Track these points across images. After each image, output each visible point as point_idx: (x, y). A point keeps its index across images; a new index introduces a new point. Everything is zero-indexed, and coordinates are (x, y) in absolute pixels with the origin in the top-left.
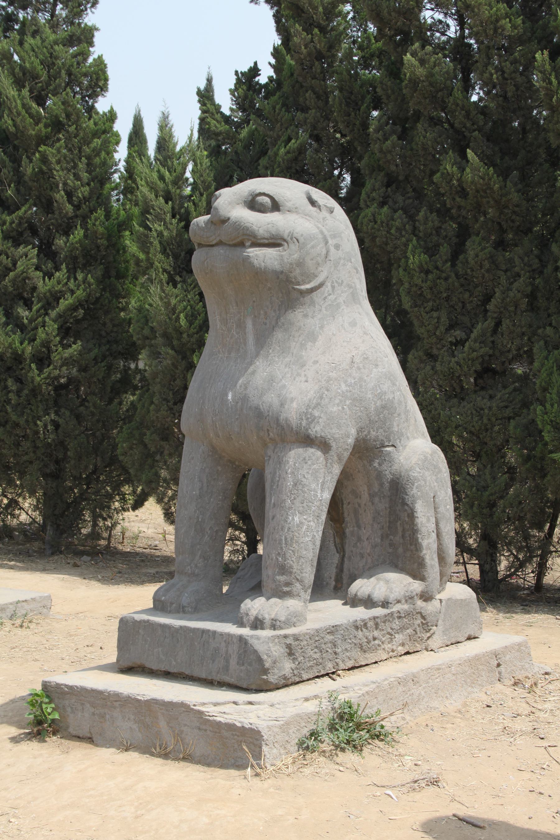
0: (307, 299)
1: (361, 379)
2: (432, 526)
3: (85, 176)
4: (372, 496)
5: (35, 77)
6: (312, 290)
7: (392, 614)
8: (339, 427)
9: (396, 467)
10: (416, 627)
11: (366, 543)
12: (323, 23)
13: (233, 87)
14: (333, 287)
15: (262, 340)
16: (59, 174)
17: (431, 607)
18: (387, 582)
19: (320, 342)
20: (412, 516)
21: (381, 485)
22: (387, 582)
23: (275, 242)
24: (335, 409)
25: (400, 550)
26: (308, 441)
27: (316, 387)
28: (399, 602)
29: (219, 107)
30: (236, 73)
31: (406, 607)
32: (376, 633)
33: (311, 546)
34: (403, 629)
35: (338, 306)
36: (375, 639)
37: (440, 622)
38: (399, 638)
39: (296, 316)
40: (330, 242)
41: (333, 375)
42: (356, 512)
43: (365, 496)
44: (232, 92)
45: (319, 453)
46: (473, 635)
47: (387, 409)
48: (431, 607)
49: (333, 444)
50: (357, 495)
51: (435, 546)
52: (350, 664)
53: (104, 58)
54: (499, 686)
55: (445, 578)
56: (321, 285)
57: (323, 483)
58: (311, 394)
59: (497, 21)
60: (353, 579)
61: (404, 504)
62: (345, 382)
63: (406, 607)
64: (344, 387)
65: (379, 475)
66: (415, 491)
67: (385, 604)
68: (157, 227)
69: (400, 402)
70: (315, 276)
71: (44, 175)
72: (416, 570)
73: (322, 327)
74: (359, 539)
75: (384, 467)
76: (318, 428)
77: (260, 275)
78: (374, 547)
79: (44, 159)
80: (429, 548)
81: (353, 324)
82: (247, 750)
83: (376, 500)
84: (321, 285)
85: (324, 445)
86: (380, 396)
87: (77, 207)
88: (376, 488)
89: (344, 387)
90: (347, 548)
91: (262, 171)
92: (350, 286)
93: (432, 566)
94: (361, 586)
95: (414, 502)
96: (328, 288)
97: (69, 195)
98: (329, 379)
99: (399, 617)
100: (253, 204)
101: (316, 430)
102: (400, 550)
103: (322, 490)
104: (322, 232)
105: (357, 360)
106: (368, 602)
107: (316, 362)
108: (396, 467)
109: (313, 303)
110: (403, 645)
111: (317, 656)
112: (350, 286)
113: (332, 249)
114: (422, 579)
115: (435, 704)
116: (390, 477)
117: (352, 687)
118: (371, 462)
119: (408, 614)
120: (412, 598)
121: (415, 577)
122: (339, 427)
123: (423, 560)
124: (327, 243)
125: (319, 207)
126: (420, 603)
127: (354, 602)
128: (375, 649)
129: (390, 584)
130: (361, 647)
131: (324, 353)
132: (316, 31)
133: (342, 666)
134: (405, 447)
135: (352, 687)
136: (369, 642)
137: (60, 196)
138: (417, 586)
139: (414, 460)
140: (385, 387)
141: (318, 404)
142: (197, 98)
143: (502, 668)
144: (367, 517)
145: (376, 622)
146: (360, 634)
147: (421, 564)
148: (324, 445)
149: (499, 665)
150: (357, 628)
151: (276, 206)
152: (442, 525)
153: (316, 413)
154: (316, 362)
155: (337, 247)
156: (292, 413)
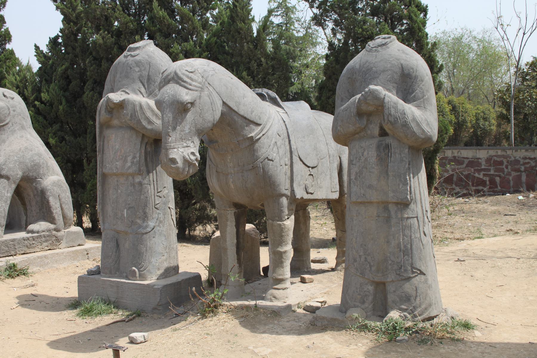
0: (2, 128)
1: (23, 155)
2: (58, 205)
4: (34, 195)
6: (3, 126)
7: (41, 236)
8: (13, 171)
9: (42, 186)
10: (53, 241)
11: (34, 212)
12: (75, 21)
13: (48, 44)
14: (13, 125)
17: (59, 234)
18: (40, 225)
19: (7, 143)
20: (48, 202)
21: (37, 192)
22: (40, 225)
24: (12, 165)
25: (46, 214)
27: (4, 158)
28: (44, 231)
29: (42, 51)
30: (50, 38)
31: (47, 233)
32: (34, 242)
33: (3, 212)
34: (46, 241)
35: (15, 131)
36: (33, 244)
37: (64, 239)
38: (45, 244)
40: (11, 109)
41: (12, 154)
42: (30, 201)
43: (32, 195)
44: (47, 46)
45: (6, 181)
46: (81, 244)
47: (36, 166)
48: (59, 234)
49: (11, 178)
50: (29, 195)
51: (60, 213)
52: (23, 252)
53: (10, 30)
54: (87, 261)
55: (66, 224)
56: (7, 124)
57: (7, 191)
58: (2, 161)
59: (127, 24)
60: (30, 224)
61: (45, 198)
62: (17, 156)
63: (47, 233)
64: (16, 158)
65: (36, 188)
66: (49, 193)
67: (38, 232)
69: (43, 163)
70: (5, 121)
72: (52, 220)
73: (8, 138)
74: (32, 211)
75: (38, 185)
76: (4, 172)
78: (37, 213)
80: (56, 213)
81: (22, 137)
82: (253, 303)
83: (36, 197)
84: (7, 124)
85: (7, 178)
86: (33, 161)
88: (36, 193)
89: (16, 158)
90: (28, 214)
91: (172, 57)
92: (20, 124)
93: (59, 220)
94: (31, 227)
95: (48, 197)
96: (10, 124)
98: (10, 156)
99: (44, 237)
102: (46, 214)
103: (7, 193)
104: (7, 106)
105: (22, 149)
106: (32, 232)
107: (5, 150)
108: (42, 186)
109: (4, 130)
110: (47, 246)
111: (7, 249)
112: (20, 124)
113: (12, 112)
114: (55, 224)
115: (55, 265)
116: (40, 189)
117: (18, 260)
118: (32, 184)
119: (48, 236)
120: (50, 230)
121: (52, 223)
122: (13, 171)
123: (54, 217)
124: (9, 109)
125: (7, 97)
126: (54, 232)
127: (28, 232)
128: (34, 247)
129: (41, 226)
130: (27, 247)
131: (8, 147)
132: (72, 24)
133: (19, 253)
134: (46, 179)
135: (18, 260)
136: (30, 245)
138: (52, 226)
139: (49, 183)
140: (35, 158)
141: (4, 164)
142: (34, 47)
143: (89, 255)
144: (34, 203)
145: (37, 237)
146: (26, 242)
147: (54, 219)
149: (87, 254)
150: (24, 240)
152: (63, 206)
153: (4, 167)
154: (5, 150)
155: (14, 111)
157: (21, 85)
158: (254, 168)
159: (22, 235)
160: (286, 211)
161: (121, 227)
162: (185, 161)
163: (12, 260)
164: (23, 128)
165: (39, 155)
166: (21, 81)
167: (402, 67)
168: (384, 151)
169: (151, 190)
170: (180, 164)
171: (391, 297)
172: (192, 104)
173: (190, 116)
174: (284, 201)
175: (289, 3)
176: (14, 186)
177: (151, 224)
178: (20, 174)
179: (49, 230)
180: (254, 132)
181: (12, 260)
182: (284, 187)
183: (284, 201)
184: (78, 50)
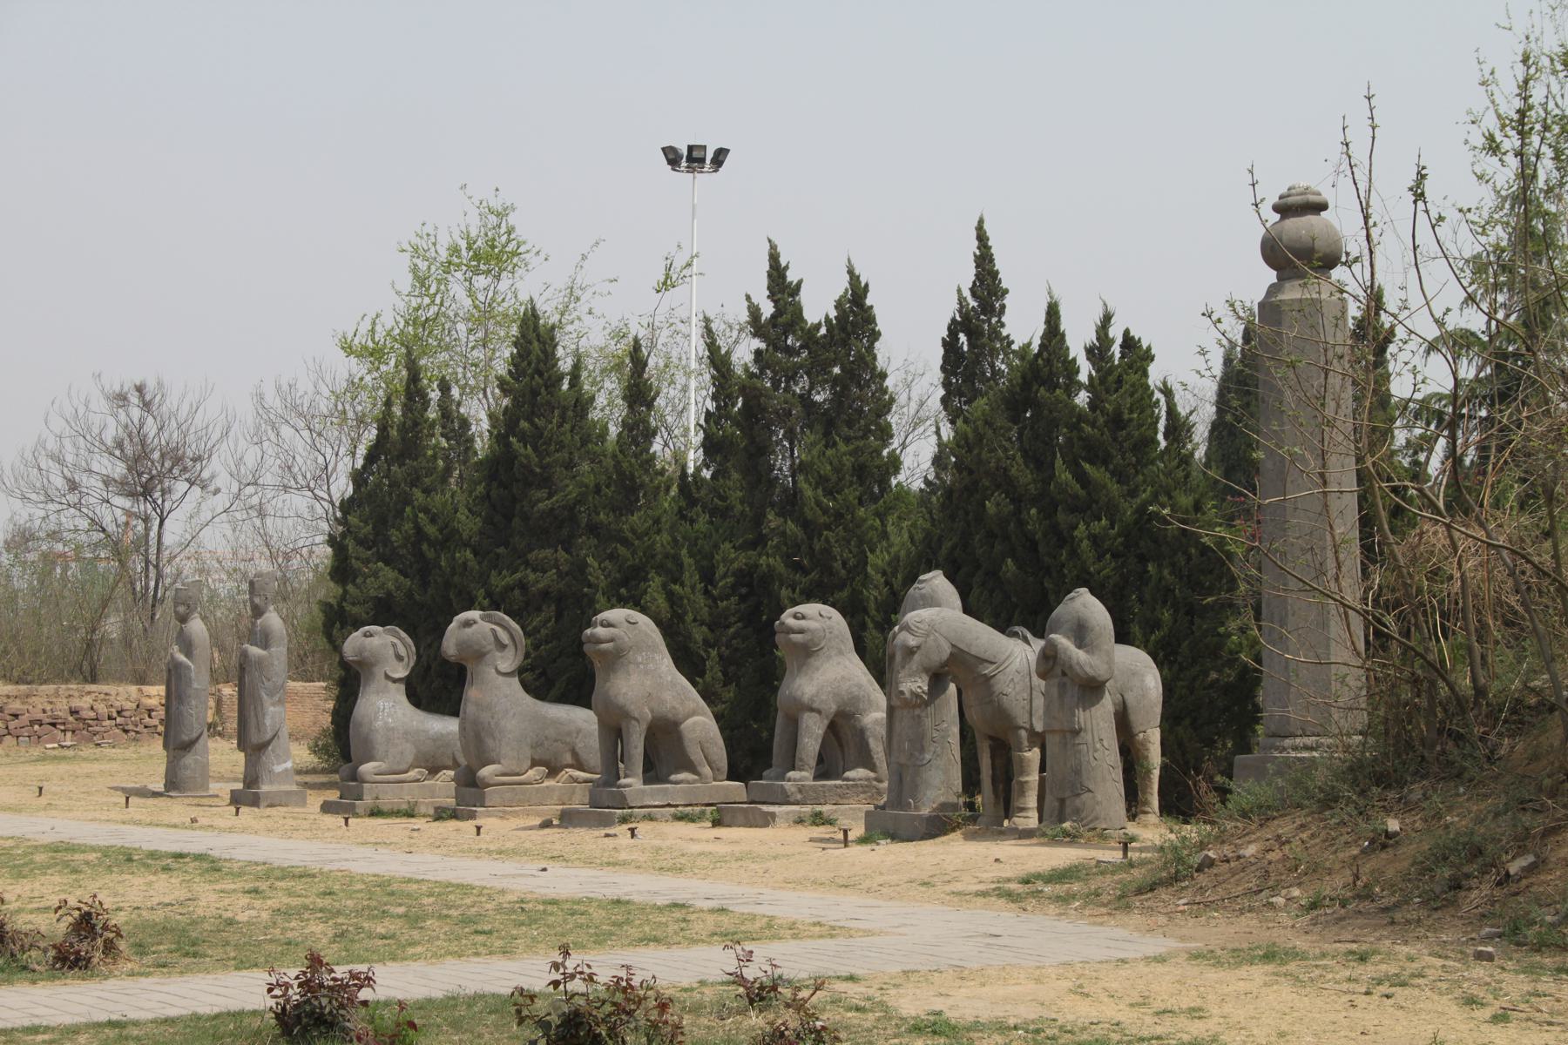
3: (855, 550)
5: (827, 480)
15: (799, 670)
16: (836, 550)
20: (867, 744)
23: (801, 631)
26: (812, 710)
39: (812, 660)
47: (855, 699)
68: (875, 593)
71: (827, 551)
72: (873, 768)
77: (795, 645)
79: (827, 541)
85: (819, 712)
87: (849, 572)
94: (848, 774)
97: (844, 564)
100: (795, 617)
101: (815, 705)
106: (847, 779)
117: (825, 809)
129: (859, 773)
137: (838, 565)
138: (872, 775)
148: (819, 712)
151: (803, 618)
156: (806, 698)
157: (889, 570)
158: (991, 702)
159: (839, 782)
160: (1026, 743)
161: (903, 760)
162: (912, 693)
163: (818, 808)
164: (840, 653)
165: (860, 686)
166: (889, 564)
167: (269, 743)
168: (1062, 686)
169: (928, 722)
170: (907, 695)
171: (1068, 810)
172: (918, 647)
173: (916, 657)
174: (1023, 733)
175: (1552, 349)
176: (826, 722)
177: (928, 757)
178: (834, 708)
179: (868, 779)
180: (988, 670)
181: (818, 808)
182: (1022, 719)
183: (1023, 733)
184: (971, 517)
